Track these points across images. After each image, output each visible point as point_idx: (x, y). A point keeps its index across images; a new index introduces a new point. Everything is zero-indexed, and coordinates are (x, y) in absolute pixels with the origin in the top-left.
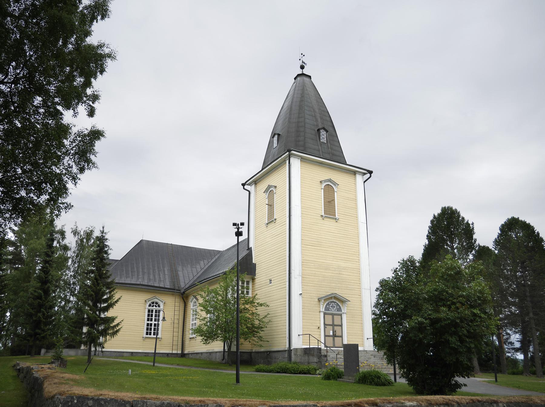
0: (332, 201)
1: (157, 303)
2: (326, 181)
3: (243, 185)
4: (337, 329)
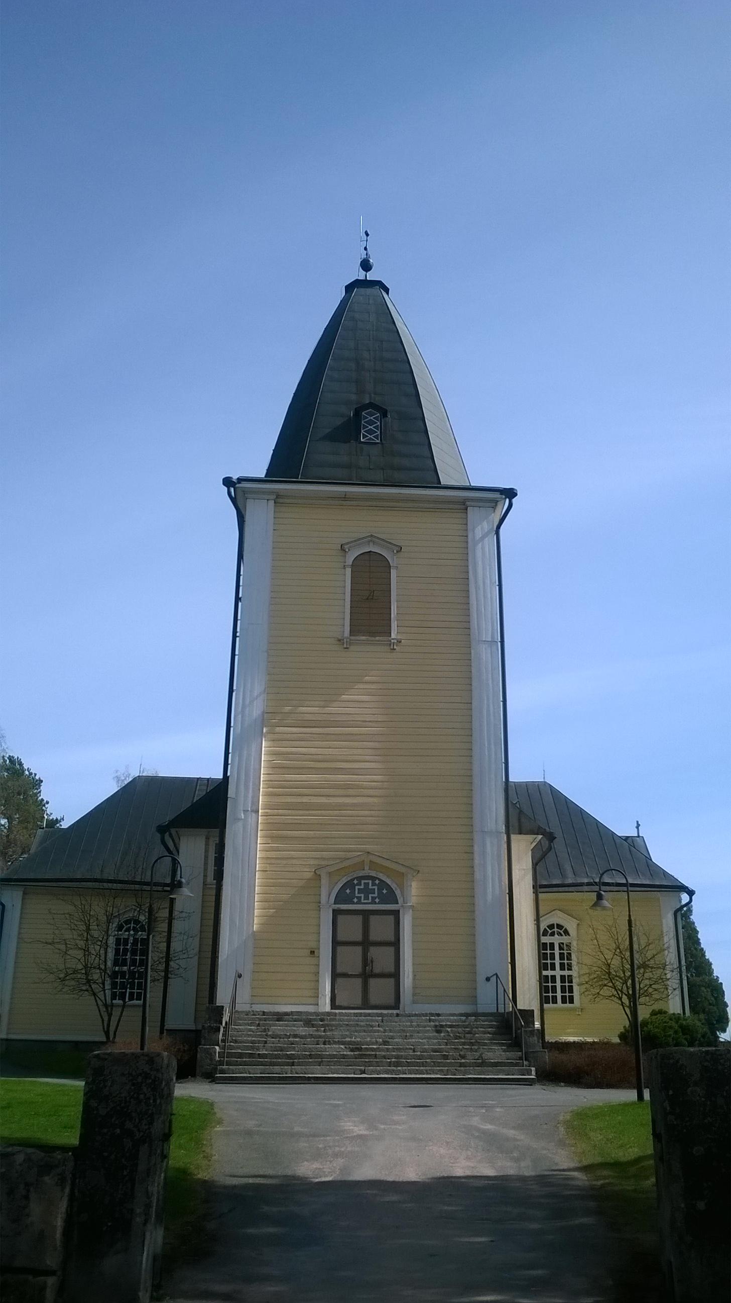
1: (560, 927)
2: (358, 541)
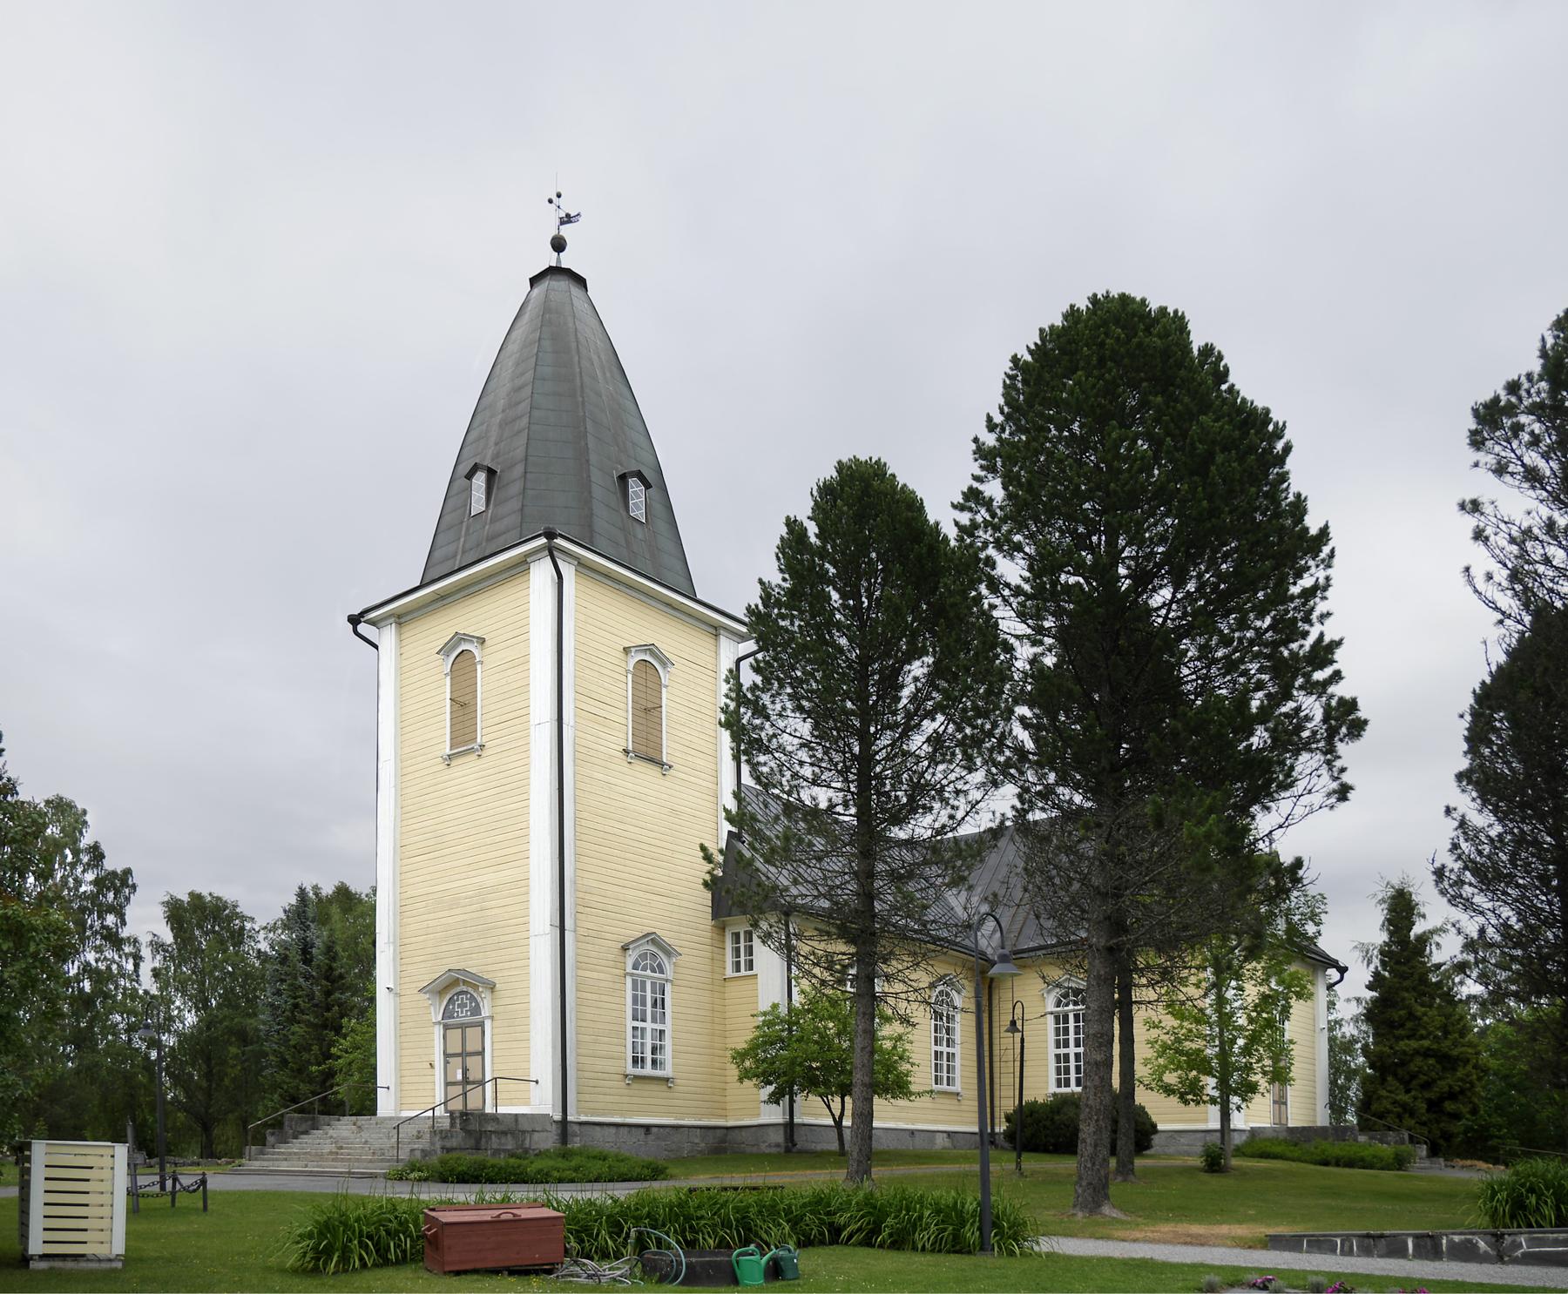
0: (654, 708)
3: (354, 620)
4: (472, 1062)
